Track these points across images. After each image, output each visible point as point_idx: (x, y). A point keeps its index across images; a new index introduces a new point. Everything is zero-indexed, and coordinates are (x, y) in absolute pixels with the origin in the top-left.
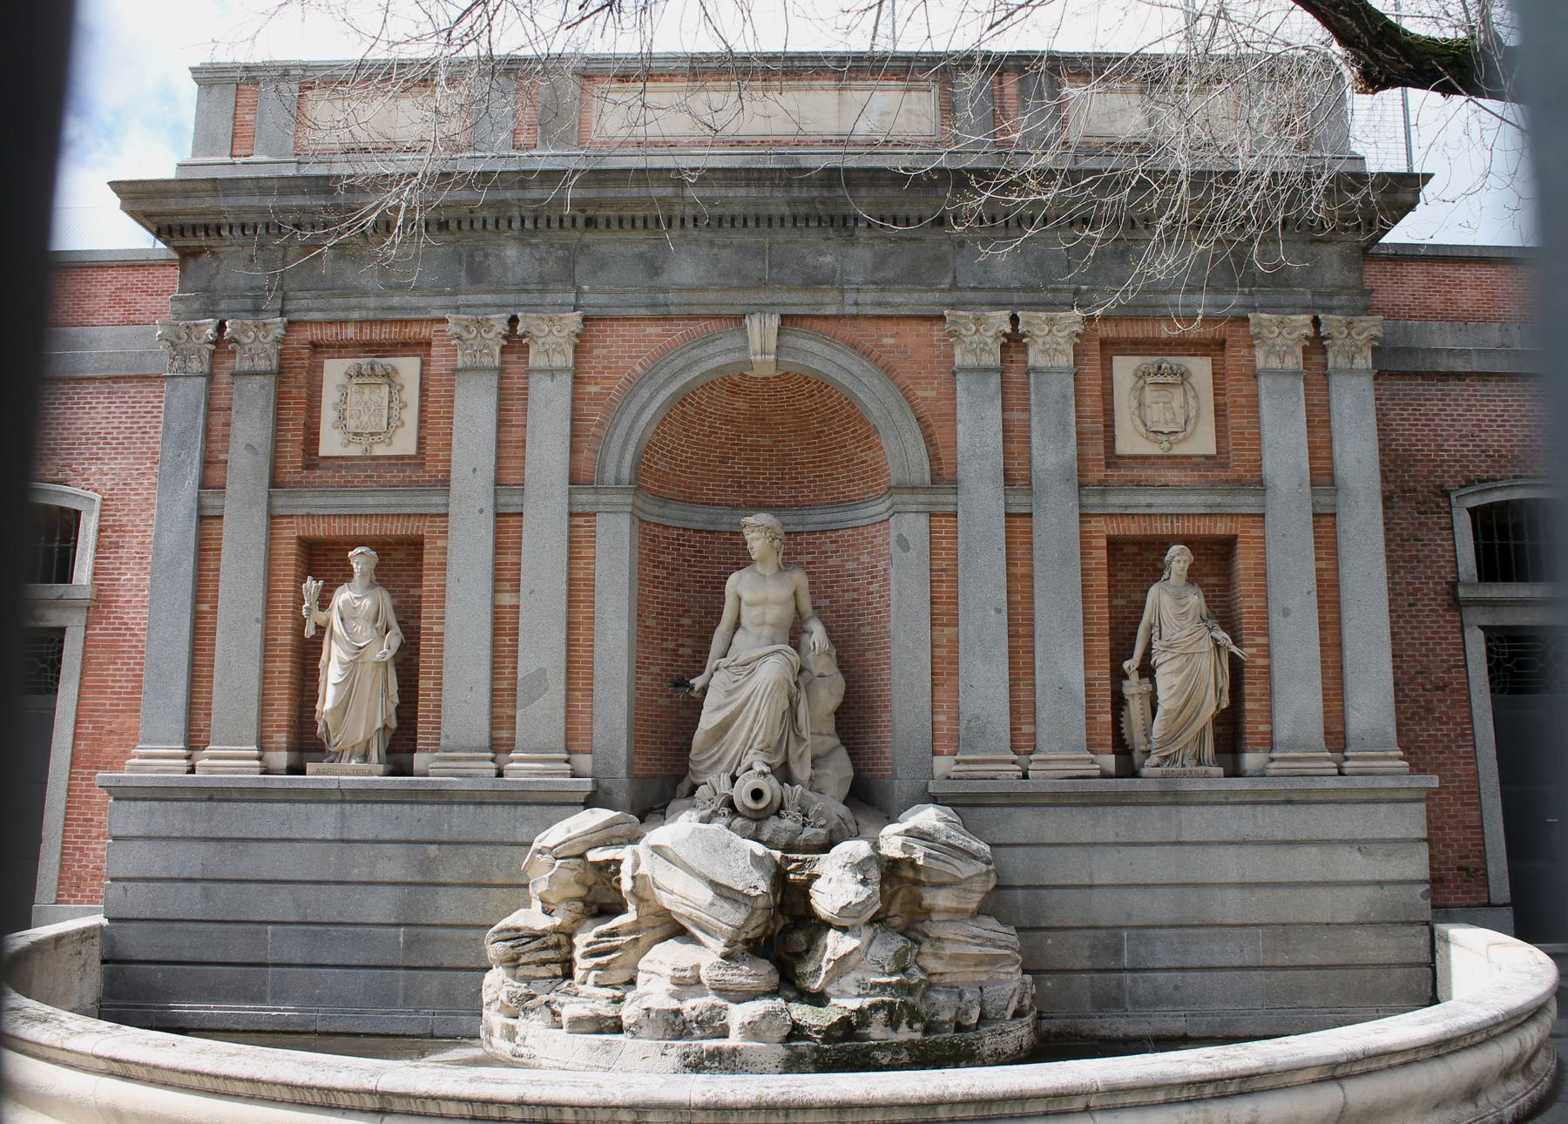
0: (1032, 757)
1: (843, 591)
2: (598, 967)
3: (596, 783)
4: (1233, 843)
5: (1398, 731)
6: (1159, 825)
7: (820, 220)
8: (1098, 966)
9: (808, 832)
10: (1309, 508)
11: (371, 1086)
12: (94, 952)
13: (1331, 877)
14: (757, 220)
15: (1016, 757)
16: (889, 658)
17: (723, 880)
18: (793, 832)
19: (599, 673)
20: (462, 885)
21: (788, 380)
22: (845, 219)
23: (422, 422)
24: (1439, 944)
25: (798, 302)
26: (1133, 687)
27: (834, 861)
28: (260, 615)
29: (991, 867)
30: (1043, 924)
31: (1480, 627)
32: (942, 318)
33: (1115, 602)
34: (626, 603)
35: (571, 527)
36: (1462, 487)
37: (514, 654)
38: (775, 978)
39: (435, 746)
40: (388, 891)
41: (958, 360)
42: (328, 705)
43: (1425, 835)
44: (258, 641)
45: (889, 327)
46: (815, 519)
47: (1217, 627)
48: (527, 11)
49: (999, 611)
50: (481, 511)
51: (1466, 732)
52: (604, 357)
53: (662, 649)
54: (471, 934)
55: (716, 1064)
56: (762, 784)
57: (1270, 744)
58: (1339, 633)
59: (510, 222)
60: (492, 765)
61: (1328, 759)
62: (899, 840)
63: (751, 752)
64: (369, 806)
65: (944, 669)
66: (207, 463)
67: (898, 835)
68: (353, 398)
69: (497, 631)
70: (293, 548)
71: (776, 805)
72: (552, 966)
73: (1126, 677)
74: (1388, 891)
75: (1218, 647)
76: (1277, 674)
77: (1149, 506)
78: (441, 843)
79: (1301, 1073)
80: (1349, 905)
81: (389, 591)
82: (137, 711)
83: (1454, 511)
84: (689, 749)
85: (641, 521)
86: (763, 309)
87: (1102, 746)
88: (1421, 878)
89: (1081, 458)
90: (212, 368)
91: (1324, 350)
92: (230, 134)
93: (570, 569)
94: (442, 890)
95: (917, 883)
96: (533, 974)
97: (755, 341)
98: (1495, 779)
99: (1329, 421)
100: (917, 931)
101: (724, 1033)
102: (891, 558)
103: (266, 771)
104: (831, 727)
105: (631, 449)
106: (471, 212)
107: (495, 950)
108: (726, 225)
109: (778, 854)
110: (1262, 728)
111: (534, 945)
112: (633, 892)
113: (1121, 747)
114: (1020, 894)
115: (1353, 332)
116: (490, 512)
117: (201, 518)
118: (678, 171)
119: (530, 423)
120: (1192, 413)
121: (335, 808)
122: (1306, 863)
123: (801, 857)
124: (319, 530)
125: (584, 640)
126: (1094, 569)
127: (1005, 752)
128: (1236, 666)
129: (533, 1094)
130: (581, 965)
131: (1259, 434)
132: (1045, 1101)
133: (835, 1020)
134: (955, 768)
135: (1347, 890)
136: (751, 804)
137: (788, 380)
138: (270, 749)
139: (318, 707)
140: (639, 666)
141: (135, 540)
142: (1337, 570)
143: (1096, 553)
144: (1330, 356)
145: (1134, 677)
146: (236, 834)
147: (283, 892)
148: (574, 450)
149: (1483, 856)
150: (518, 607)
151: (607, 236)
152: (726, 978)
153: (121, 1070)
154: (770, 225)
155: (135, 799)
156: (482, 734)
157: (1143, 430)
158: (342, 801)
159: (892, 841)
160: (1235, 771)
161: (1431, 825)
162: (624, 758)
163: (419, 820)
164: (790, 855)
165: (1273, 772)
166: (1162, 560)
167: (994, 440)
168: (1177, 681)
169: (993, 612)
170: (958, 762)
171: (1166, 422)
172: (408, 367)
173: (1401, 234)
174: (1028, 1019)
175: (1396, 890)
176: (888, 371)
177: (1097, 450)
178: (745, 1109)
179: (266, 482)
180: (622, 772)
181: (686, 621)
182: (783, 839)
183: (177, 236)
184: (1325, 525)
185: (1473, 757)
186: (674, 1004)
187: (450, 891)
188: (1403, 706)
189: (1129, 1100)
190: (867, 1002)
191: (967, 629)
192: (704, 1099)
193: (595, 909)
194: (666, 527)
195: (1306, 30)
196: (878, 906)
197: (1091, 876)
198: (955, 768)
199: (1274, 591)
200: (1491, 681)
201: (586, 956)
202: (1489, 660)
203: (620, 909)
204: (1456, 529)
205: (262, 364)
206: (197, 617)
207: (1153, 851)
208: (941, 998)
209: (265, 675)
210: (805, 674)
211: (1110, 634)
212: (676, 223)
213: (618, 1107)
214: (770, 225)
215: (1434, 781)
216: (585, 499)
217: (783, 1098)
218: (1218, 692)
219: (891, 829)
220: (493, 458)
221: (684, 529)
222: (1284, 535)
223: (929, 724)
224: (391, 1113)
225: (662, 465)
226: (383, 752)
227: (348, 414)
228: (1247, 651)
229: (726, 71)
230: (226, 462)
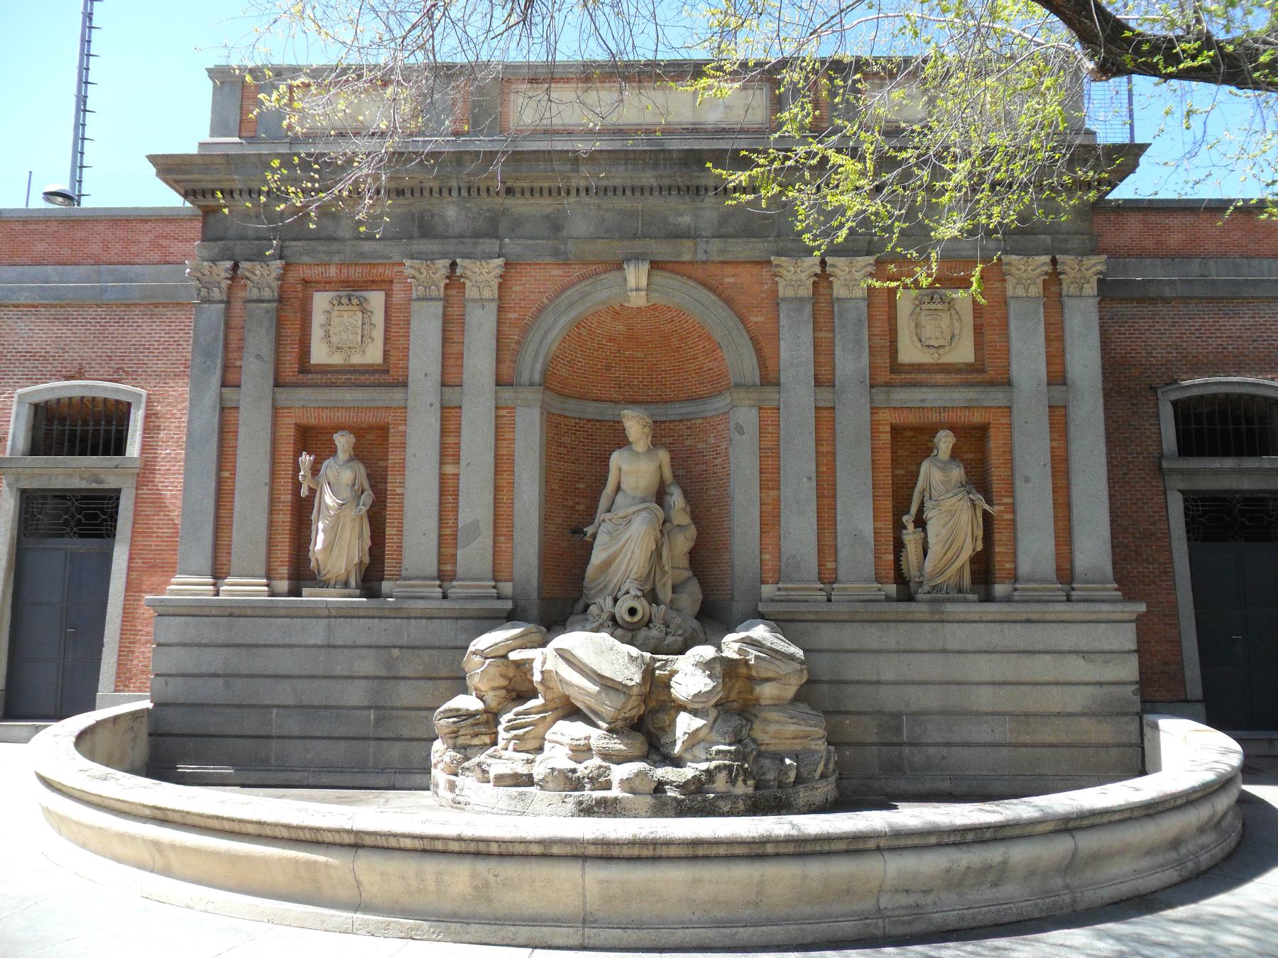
0: (834, 586)
1: (696, 464)
2: (515, 737)
3: (515, 603)
4: (986, 652)
5: (1114, 568)
6: (929, 637)
7: (679, 189)
8: (884, 741)
9: (670, 639)
10: (1045, 402)
11: (348, 827)
12: (144, 729)
13: (1061, 678)
14: (633, 190)
15: (822, 586)
16: (729, 513)
17: (607, 674)
18: (658, 639)
19: (517, 523)
20: (417, 678)
21: (655, 310)
22: (698, 189)
23: (387, 340)
24: (1147, 730)
25: (661, 249)
26: (911, 537)
27: (689, 660)
28: (267, 480)
29: (804, 667)
31: (1179, 491)
32: (769, 262)
33: (897, 472)
34: (537, 472)
35: (497, 417)
36: (1167, 384)
37: (456, 509)
38: (645, 747)
39: (399, 577)
40: (362, 683)
41: (781, 294)
42: (319, 546)
43: (1135, 647)
44: (266, 500)
45: (729, 270)
46: (675, 411)
47: (974, 491)
48: (460, 24)
49: (810, 478)
50: (431, 405)
51: (1167, 570)
52: (520, 292)
53: (564, 506)
54: (424, 713)
55: (603, 810)
56: (636, 604)
57: (1015, 579)
58: (1069, 495)
59: (450, 191)
60: (440, 590)
61: (1059, 590)
62: (736, 646)
63: (628, 581)
64: (349, 620)
65: (770, 521)
66: (226, 368)
67: (735, 641)
68: (335, 320)
69: (442, 492)
70: (291, 432)
71: (646, 619)
72: (483, 737)
73: (905, 527)
74: (1105, 689)
75: (974, 506)
76: (1019, 525)
77: (923, 401)
78: (401, 647)
79: (1042, 825)
80: (1076, 700)
81: (364, 463)
82: (175, 550)
83: (1160, 403)
84: (583, 579)
85: (549, 413)
86: (637, 258)
89: (872, 366)
90: (229, 297)
91: (1060, 282)
92: (238, 121)
93: (496, 447)
94: (402, 682)
95: (750, 679)
96: (468, 742)
97: (632, 282)
98: (1190, 606)
99: (1062, 336)
100: (750, 712)
101: (608, 786)
102: (730, 440)
103: (272, 594)
104: (685, 562)
105: (541, 360)
106: (421, 182)
107: (442, 724)
108: (610, 194)
109: (648, 655)
110: (1008, 566)
111: (470, 721)
112: (543, 682)
113: (900, 578)
114: (825, 688)
115: (1083, 268)
116: (437, 405)
117: (223, 409)
118: (575, 152)
119: (466, 340)
120: (957, 332)
121: (323, 622)
122: (1042, 668)
123: (664, 657)
124: (311, 419)
125: (508, 499)
126: (880, 448)
127: (814, 582)
128: (987, 517)
129: (468, 832)
130: (502, 735)
131: (1008, 346)
132: (846, 842)
133: (689, 777)
134: (778, 593)
135: (1074, 688)
136: (628, 618)
137: (655, 310)
138: (275, 579)
139: (311, 548)
140: (546, 518)
141: (173, 425)
142: (1067, 449)
143: (883, 436)
144: (1064, 287)
145: (911, 527)
146: (250, 641)
147: (285, 685)
148: (499, 361)
149: (1180, 663)
150: (458, 475)
151: (522, 201)
152: (610, 746)
153: (162, 817)
154: (642, 194)
155: (174, 615)
156: (431, 567)
157: (918, 345)
158: (329, 617)
159: (731, 645)
160: (988, 598)
161: (1141, 638)
162: (536, 585)
163: (386, 630)
164: (656, 656)
165: (1016, 598)
166: (932, 441)
167: (807, 353)
168: (944, 532)
169: (805, 480)
170: (779, 589)
172: (376, 299)
173: (1124, 191)
174: (833, 779)
175: (1113, 689)
176: (728, 302)
177: (884, 361)
178: (624, 844)
179: (271, 382)
180: (535, 595)
181: (581, 486)
182: (652, 643)
183: (200, 197)
184: (1059, 419)
185: (1172, 589)
186: (572, 765)
187: (408, 682)
188: (1118, 550)
189: (910, 842)
190: (713, 764)
191: (787, 491)
192: (594, 836)
193: (514, 695)
194: (567, 417)
195: (1058, 35)
196: (720, 695)
197: (878, 673)
198: (778, 593)
199: (1019, 463)
200: (1188, 532)
201: (507, 730)
202: (1186, 515)
203: (534, 695)
204: (1161, 417)
205: (267, 294)
206: (220, 482)
207: (926, 657)
208: (767, 763)
209: (271, 524)
210: (668, 524)
211: (893, 496)
212: (573, 192)
213: (530, 842)
214: (642, 194)
215: (1142, 608)
216: (507, 394)
217: (651, 836)
218: (974, 538)
219: (729, 638)
220: (440, 366)
221: (580, 419)
223: (758, 561)
224: (363, 846)
225: (563, 372)
226: (359, 581)
227: (331, 334)
228: (996, 508)
229: (611, 74)
230: (241, 367)
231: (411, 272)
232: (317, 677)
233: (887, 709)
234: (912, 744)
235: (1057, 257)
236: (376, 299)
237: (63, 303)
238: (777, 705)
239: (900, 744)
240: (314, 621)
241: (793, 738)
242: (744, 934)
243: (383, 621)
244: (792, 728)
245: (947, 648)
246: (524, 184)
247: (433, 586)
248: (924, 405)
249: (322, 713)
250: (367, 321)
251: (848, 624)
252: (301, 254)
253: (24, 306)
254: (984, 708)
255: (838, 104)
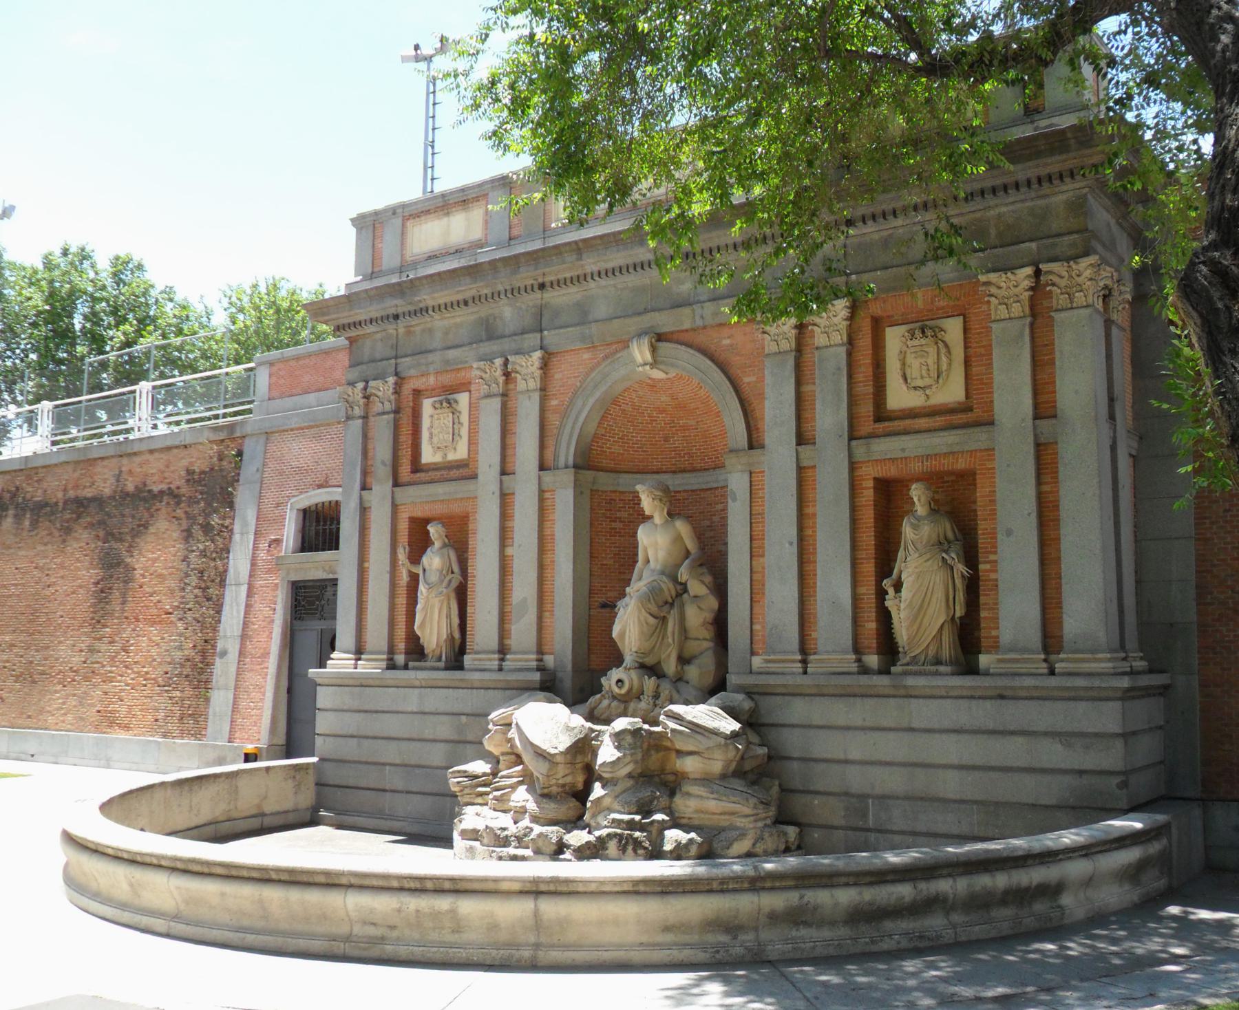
12: (311, 779)
25: (665, 321)
30: (812, 788)
39: (995, 647)
49: (791, 544)
60: (1045, 665)
77: (903, 450)
78: (468, 715)
87: (870, 648)
88: (1117, 769)
116: (498, 493)
120: (944, 367)
121: (417, 691)
143: (866, 492)
147: (393, 745)
156: (494, 644)
160: (971, 669)
169: (787, 545)
171: (922, 377)
179: (391, 483)
198: (765, 665)
222: (1008, 466)
231: (478, 373)
232: (413, 740)
233: (853, 791)
234: (879, 831)
235: (1041, 266)
236: (953, 328)
237: (318, 423)
238: (706, 780)
239: (868, 830)
240: (411, 690)
241: (721, 814)
242: (250, 939)
243: (456, 690)
244: (712, 805)
245: (913, 725)
246: (884, 207)
247: (490, 660)
248: (906, 454)
249: (417, 771)
250: (456, 420)
251: (818, 698)
252: (410, 368)
253: (298, 429)
254: (951, 796)
255: (63, 321)
